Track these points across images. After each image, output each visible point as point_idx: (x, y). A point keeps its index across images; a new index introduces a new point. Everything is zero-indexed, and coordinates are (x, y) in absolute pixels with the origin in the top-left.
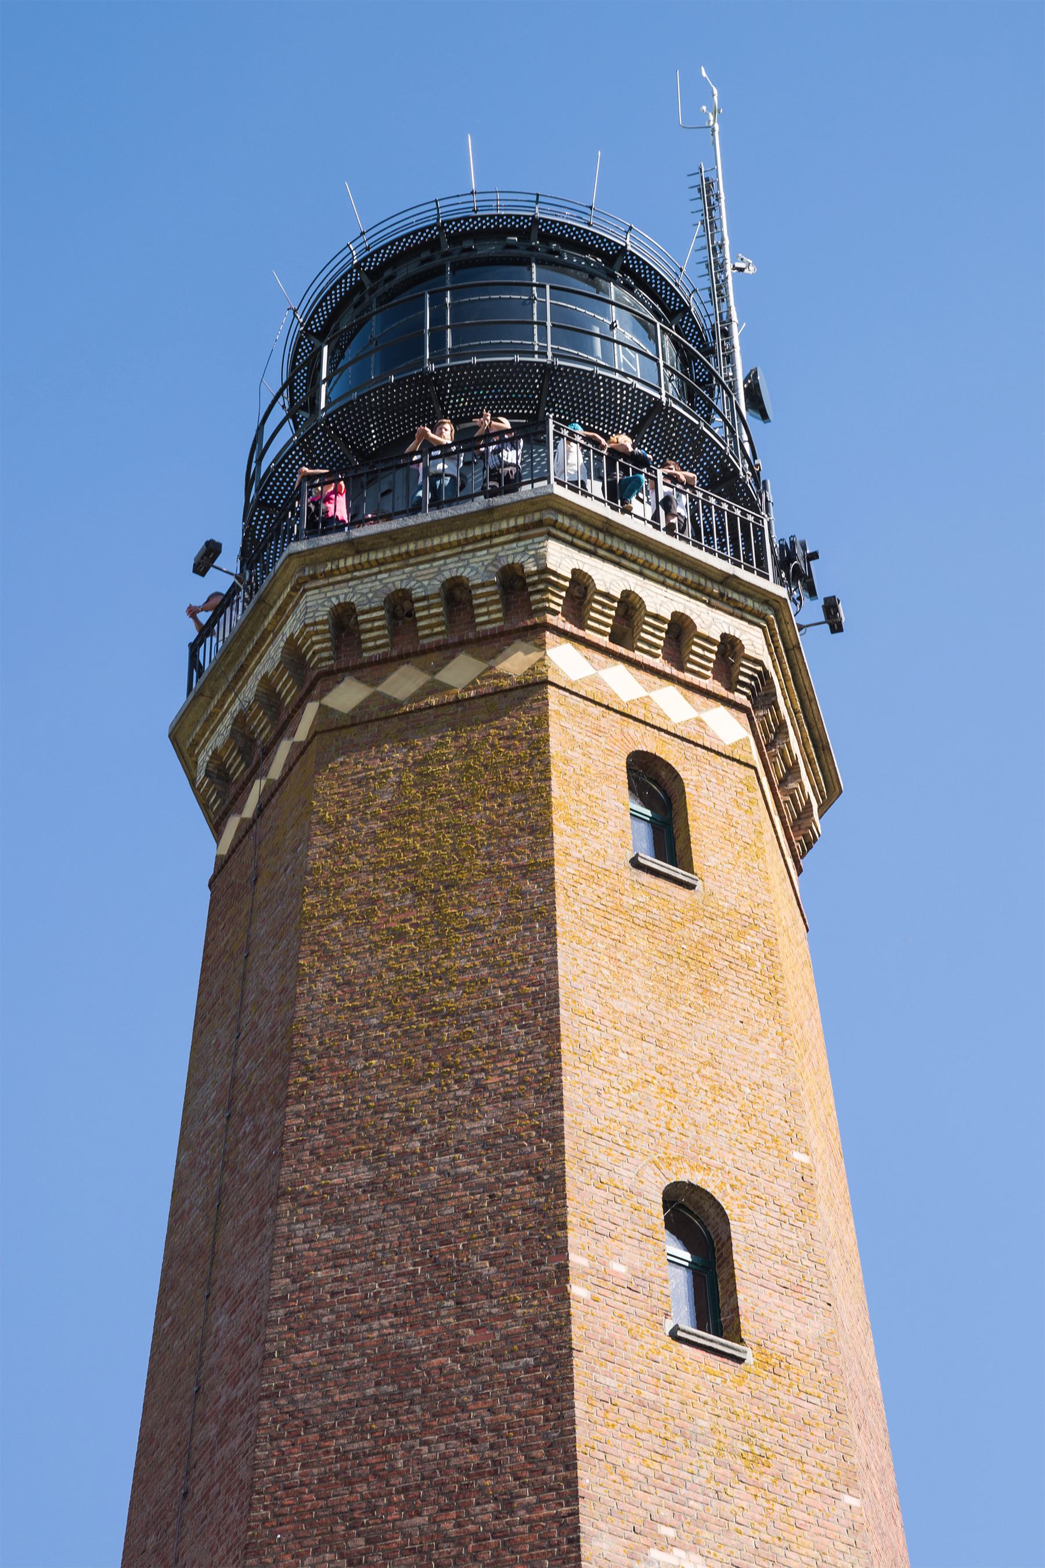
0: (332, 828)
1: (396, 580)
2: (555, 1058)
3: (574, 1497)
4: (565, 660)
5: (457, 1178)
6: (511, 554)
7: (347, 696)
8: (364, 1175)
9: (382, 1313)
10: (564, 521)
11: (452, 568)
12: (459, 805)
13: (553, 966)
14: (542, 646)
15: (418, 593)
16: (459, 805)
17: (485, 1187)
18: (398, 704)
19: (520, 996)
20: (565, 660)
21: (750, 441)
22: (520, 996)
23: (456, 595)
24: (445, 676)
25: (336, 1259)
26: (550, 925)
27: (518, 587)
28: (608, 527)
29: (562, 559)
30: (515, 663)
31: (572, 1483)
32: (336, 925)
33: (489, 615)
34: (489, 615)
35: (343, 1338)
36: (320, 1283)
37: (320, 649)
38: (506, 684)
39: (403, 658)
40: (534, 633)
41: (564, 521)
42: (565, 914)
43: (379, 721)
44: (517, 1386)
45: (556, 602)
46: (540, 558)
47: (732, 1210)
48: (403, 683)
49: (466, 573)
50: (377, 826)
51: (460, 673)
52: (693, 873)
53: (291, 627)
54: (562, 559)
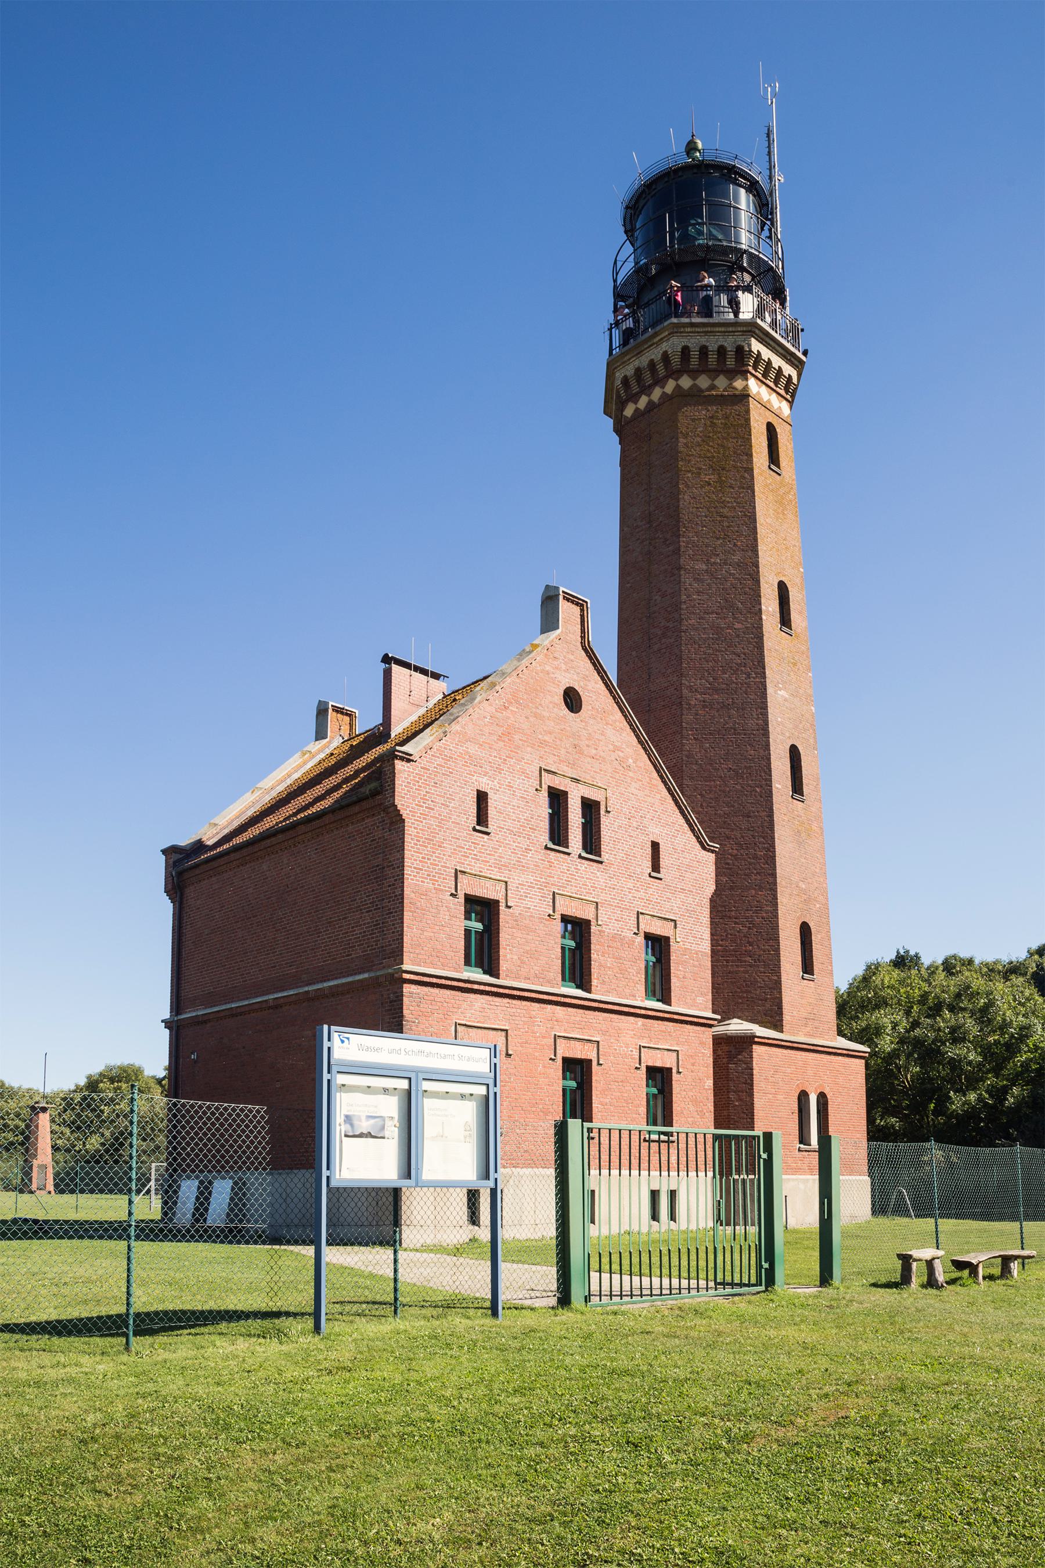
0: (686, 436)
1: (703, 340)
2: (756, 540)
3: (765, 678)
4: (753, 385)
5: (730, 574)
6: (740, 340)
7: (686, 382)
8: (704, 567)
9: (712, 613)
10: (757, 331)
11: (722, 341)
12: (724, 438)
13: (754, 507)
14: (747, 379)
15: (710, 348)
16: (724, 438)
17: (739, 579)
18: (702, 391)
19: (746, 515)
20: (753, 385)
21: (783, 268)
22: (746, 515)
23: (722, 351)
24: (716, 382)
25: (698, 593)
26: (753, 492)
27: (742, 354)
28: (767, 334)
29: (756, 346)
30: (739, 384)
31: (764, 673)
32: (689, 475)
33: (731, 363)
34: (731, 363)
35: (703, 618)
36: (695, 600)
37: (676, 361)
38: (737, 393)
39: (703, 372)
40: (744, 374)
41: (757, 331)
42: (757, 488)
43: (694, 396)
44: (750, 643)
45: (751, 363)
46: (750, 345)
47: (790, 589)
48: (703, 382)
49: (726, 344)
50: (699, 439)
51: (721, 382)
52: (779, 467)
53: (665, 346)
54: (756, 346)
